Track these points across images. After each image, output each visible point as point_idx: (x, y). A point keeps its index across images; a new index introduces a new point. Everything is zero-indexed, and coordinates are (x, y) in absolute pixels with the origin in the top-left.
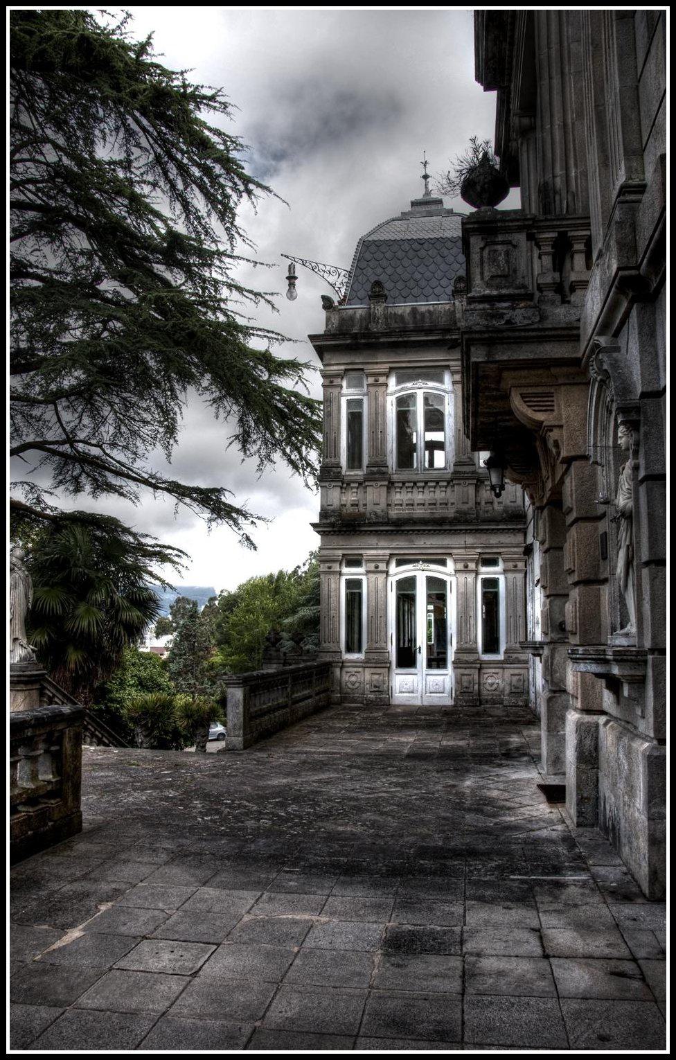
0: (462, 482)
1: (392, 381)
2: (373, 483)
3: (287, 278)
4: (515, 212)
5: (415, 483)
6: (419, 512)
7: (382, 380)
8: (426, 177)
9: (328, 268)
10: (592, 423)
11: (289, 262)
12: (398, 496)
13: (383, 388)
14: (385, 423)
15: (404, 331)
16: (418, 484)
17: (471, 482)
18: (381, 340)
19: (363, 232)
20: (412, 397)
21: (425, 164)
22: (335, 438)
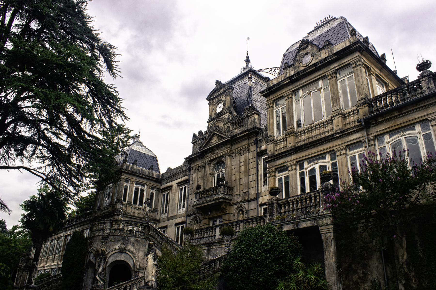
6: (136, 215)
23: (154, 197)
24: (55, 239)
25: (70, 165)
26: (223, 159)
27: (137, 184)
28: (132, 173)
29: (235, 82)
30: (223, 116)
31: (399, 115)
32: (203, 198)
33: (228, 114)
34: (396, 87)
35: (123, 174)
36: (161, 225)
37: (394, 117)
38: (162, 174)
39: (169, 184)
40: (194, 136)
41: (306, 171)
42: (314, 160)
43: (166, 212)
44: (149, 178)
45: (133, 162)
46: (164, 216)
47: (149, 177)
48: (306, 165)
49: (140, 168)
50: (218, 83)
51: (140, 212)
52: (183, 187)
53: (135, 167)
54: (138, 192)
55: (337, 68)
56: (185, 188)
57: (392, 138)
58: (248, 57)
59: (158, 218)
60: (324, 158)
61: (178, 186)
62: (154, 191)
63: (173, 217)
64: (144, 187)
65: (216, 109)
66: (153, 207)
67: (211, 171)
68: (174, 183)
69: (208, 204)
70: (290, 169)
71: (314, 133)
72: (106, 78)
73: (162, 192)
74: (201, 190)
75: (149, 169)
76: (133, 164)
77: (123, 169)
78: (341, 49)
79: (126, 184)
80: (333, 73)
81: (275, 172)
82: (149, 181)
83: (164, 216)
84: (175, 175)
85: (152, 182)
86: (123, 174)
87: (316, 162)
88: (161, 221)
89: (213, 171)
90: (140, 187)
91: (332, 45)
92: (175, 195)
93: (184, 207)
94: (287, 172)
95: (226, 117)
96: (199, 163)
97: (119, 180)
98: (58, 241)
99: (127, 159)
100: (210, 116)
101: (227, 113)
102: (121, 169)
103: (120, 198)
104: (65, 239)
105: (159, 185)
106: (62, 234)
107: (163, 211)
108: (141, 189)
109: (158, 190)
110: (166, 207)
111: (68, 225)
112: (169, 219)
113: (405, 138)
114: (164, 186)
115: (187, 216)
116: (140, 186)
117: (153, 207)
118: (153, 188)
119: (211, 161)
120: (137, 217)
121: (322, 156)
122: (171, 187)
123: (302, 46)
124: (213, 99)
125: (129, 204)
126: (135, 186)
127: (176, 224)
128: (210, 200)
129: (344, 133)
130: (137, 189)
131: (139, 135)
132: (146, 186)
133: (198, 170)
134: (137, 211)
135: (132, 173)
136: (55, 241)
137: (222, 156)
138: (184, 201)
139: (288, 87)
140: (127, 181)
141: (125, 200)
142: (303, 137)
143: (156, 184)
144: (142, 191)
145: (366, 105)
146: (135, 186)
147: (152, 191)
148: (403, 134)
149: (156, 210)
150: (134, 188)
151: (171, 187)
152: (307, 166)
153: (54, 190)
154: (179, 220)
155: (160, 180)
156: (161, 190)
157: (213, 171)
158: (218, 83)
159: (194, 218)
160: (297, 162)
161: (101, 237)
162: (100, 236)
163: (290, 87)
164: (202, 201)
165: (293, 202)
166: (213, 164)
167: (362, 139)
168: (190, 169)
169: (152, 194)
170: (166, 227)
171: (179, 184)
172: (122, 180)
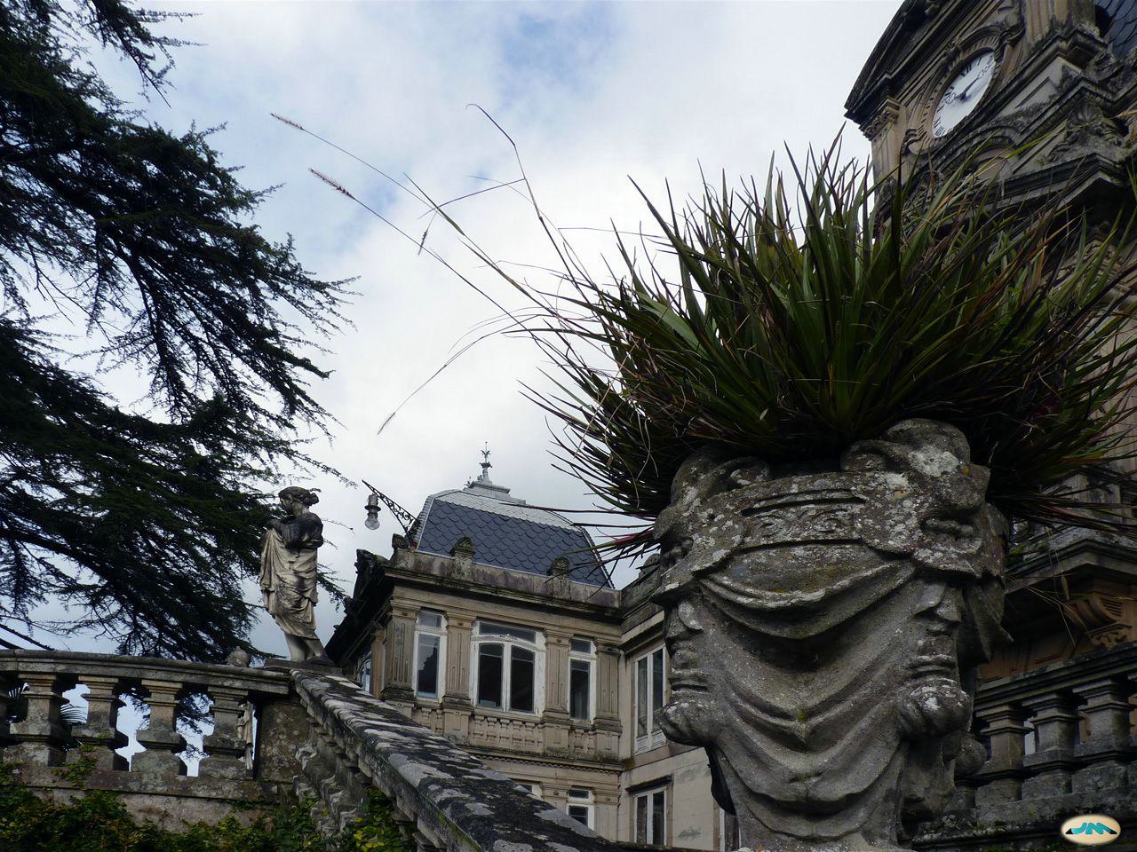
0: (555, 725)
1: (476, 630)
2: (454, 711)
3: (366, 508)
4: (385, 561)
5: (499, 720)
6: (503, 744)
7: (466, 624)
8: (486, 465)
9: (402, 511)
10: (463, 768)
11: (371, 493)
12: (478, 727)
13: (468, 633)
14: (411, 674)
15: (498, 589)
16: (514, 722)
17: (565, 727)
18: (471, 590)
19: (435, 490)
20: (498, 649)
21: (486, 454)
22: (406, 666)
25: (230, 283)
27: (484, 629)
28: (449, 586)
35: (398, 591)
36: (639, 776)
38: (624, 591)
45: (449, 548)
47: (551, 598)
49: (482, 566)
54: (499, 662)
59: (624, 753)
62: (591, 657)
64: (531, 638)
73: (628, 657)
75: (549, 573)
76: (452, 553)
79: (423, 629)
85: (569, 622)
86: (398, 591)
88: (638, 761)
90: (508, 644)
105: (615, 631)
108: (515, 651)
109: (609, 650)
116: (507, 637)
118: (581, 646)
125: (456, 702)
131: (299, 264)
135: (449, 586)
141: (428, 682)
146: (477, 639)
147: (578, 656)
153: (122, 697)
156: (624, 647)
170: (666, 781)
172: (395, 613)
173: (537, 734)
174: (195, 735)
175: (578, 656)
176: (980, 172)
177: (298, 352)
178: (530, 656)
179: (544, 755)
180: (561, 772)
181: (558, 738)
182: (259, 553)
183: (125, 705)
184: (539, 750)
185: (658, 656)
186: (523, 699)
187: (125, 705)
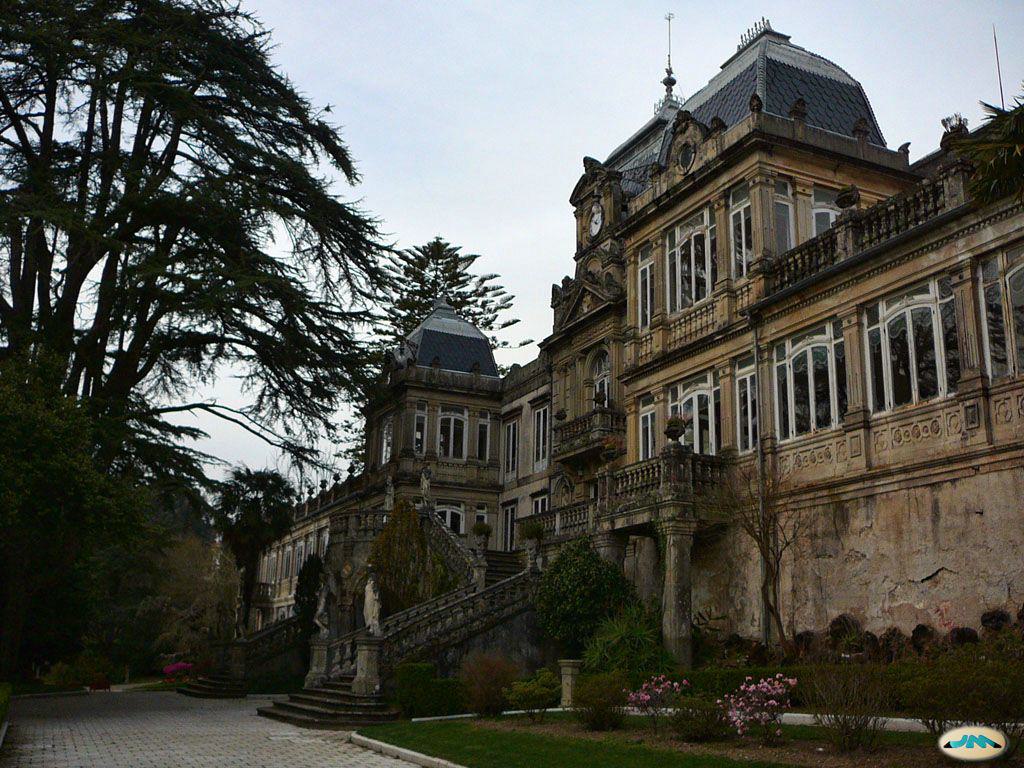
17: (723, 296)
23: (488, 434)
24: (300, 539)
26: (606, 348)
28: (431, 388)
29: (633, 151)
30: (602, 246)
31: (801, 302)
32: (567, 440)
33: (609, 241)
34: (897, 192)
37: (885, 265)
39: (515, 404)
40: (555, 287)
41: (883, 326)
42: (803, 337)
43: (513, 469)
44: (471, 392)
45: (429, 361)
46: (511, 476)
48: (883, 310)
50: (589, 162)
51: (457, 471)
52: (541, 410)
53: (436, 371)
55: (727, 186)
56: (545, 411)
57: (890, 310)
58: (669, 72)
60: (926, 290)
61: (532, 407)
62: (487, 422)
63: (525, 481)
64: (463, 413)
65: (590, 226)
66: (488, 458)
67: (586, 375)
68: (525, 400)
69: (578, 452)
70: (656, 399)
71: (696, 324)
72: (338, 187)
74: (568, 420)
77: (408, 381)
78: (735, 141)
79: (419, 413)
80: (720, 198)
81: (637, 404)
82: (471, 401)
83: (511, 476)
84: (524, 383)
85: (478, 402)
87: (693, 387)
89: (591, 373)
90: (453, 417)
91: (726, 128)
92: (528, 428)
93: (544, 457)
94: (653, 405)
95: (607, 248)
96: (565, 355)
97: (400, 407)
98: (306, 542)
99: (417, 356)
100: (579, 245)
101: (607, 239)
102: (403, 382)
103: (408, 447)
104: (319, 537)
105: (497, 404)
106: (312, 528)
107: (538, 454)
110: (513, 456)
111: (322, 506)
112: (520, 483)
113: (813, 348)
114: (506, 408)
115: (551, 478)
117: (488, 458)
118: (483, 415)
119: (586, 352)
120: (451, 483)
121: (818, 328)
122: (520, 409)
123: (678, 126)
124: (582, 202)
126: (440, 415)
127: (534, 495)
128: (579, 446)
129: (727, 333)
130: (446, 422)
132: (466, 413)
133: (565, 371)
134: (450, 471)
136: (302, 543)
137: (602, 341)
138: (544, 443)
139: (666, 215)
140: (421, 407)
142: (678, 333)
143: (490, 404)
144: (459, 423)
145: (761, 276)
146: (440, 415)
147: (482, 421)
148: (810, 341)
149: (494, 464)
150: (440, 419)
151: (520, 409)
152: (792, 350)
154: (537, 486)
155: (497, 394)
157: (591, 373)
158: (589, 162)
159: (562, 480)
160: (668, 385)
161: (342, 545)
162: (339, 543)
163: (661, 221)
164: (566, 446)
165: (632, 475)
166: (589, 358)
167: (836, 311)
168: (550, 370)
169: (483, 428)
171: (534, 403)
172: (408, 405)
173: (463, 472)
174: (296, 502)
175: (482, 421)
176: (333, 259)
177: (367, 218)
178: (462, 423)
179: (466, 485)
180: (473, 495)
181: (470, 474)
182: (734, 203)
183: (909, 144)
184: (464, 482)
185: (673, 309)
186: (458, 453)
187: (909, 144)
